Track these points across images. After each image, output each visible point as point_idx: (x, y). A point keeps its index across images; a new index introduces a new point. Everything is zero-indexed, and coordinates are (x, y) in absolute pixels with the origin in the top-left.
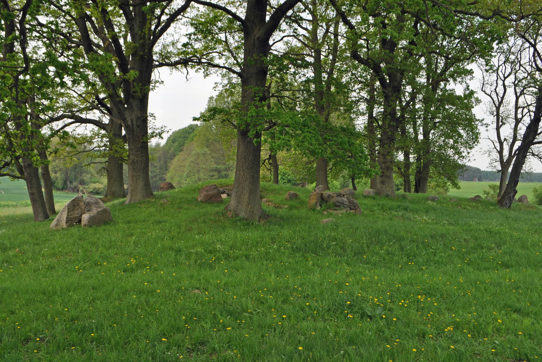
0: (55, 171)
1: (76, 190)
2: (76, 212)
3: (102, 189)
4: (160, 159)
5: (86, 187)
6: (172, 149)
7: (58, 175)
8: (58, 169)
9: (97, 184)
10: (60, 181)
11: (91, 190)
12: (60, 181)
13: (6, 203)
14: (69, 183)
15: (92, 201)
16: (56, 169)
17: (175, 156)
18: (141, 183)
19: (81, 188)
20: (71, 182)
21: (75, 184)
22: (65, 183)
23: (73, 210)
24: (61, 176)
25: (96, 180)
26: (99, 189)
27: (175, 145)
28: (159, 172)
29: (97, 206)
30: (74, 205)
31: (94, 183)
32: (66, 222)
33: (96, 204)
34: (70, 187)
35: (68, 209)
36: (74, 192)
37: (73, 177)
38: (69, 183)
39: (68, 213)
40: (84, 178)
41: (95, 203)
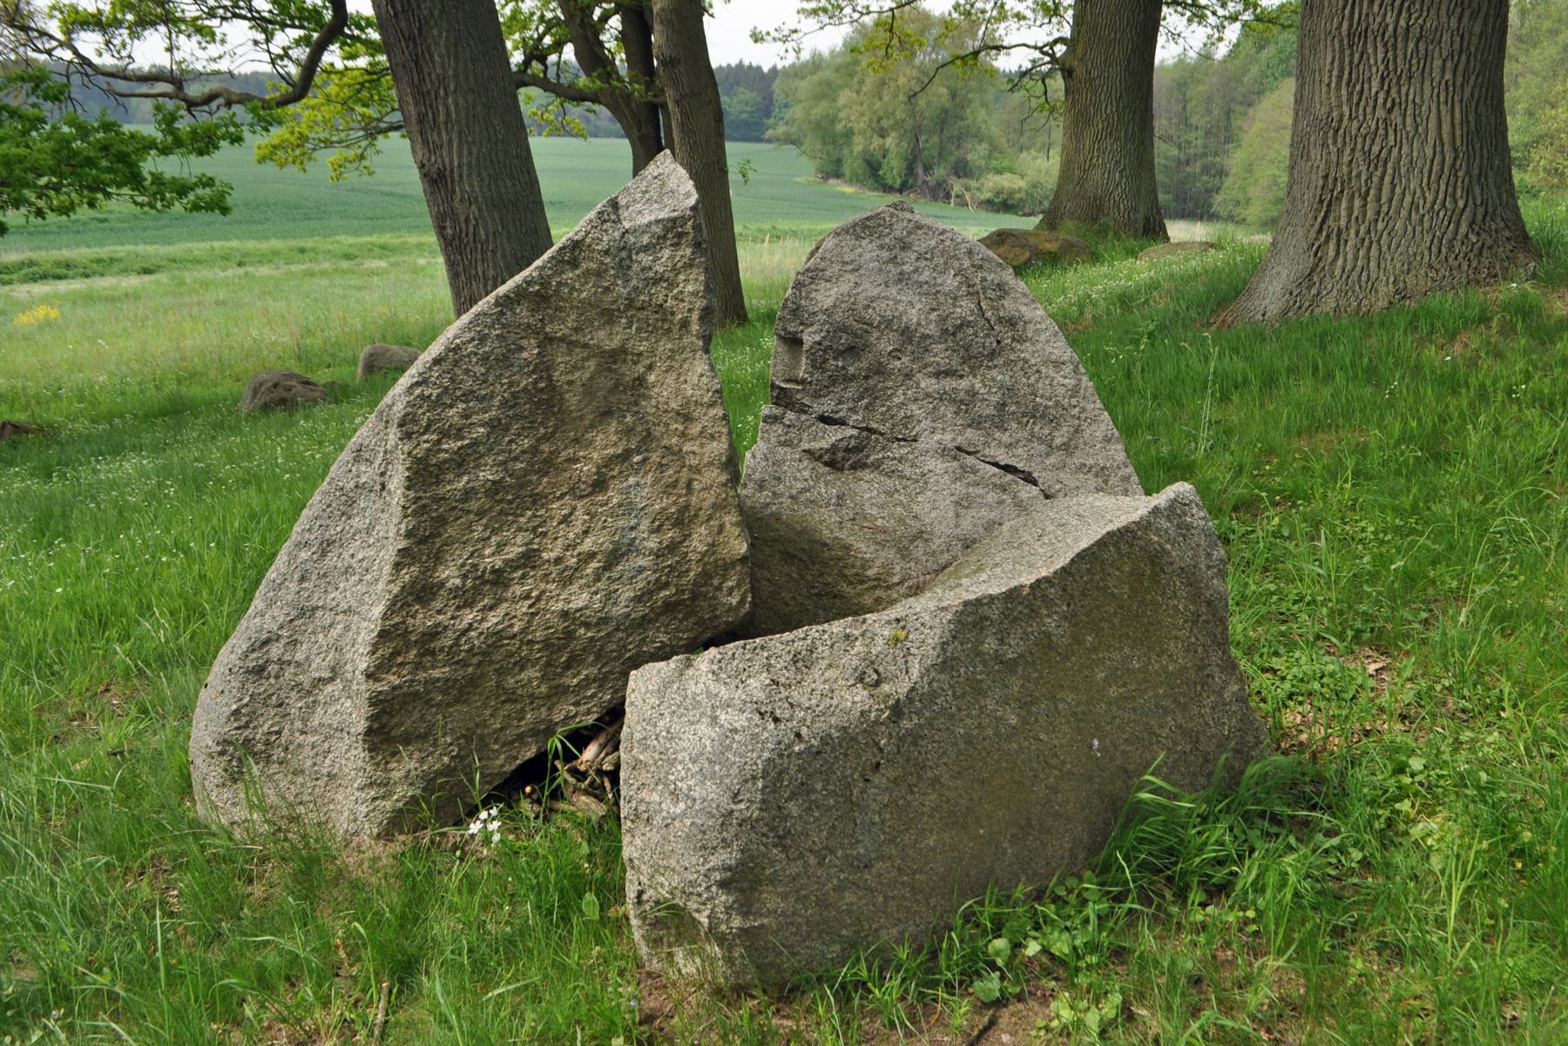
0: (882, 129)
1: (941, 194)
2: (575, 531)
3: (1022, 195)
4: (1209, 100)
5: (973, 183)
6: (1254, 70)
7: (890, 141)
8: (891, 122)
9: (1008, 175)
10: (894, 163)
11: (988, 195)
12: (894, 163)
13: (104, 252)
14: (920, 171)
15: (914, 310)
16: (885, 123)
17: (1260, 93)
18: (1432, 119)
19: (957, 187)
20: (927, 169)
21: (940, 172)
22: (910, 169)
23: (515, 498)
24: (898, 145)
25: (1006, 163)
26: (1012, 193)
27: (1265, 54)
28: (1205, 146)
29: (985, 385)
30: (543, 403)
31: (999, 172)
32: (383, 735)
33: (973, 360)
34: (925, 182)
35: (423, 474)
36: (935, 198)
37: (935, 153)
38: (920, 171)
39: (424, 544)
40: (969, 157)
41: (952, 332)
